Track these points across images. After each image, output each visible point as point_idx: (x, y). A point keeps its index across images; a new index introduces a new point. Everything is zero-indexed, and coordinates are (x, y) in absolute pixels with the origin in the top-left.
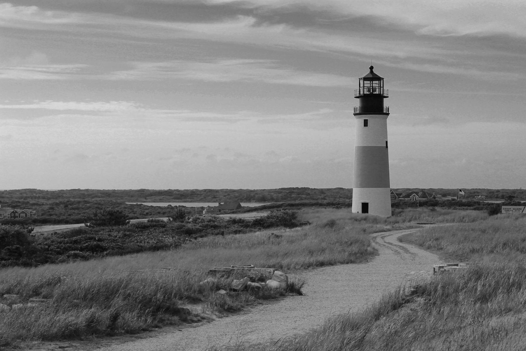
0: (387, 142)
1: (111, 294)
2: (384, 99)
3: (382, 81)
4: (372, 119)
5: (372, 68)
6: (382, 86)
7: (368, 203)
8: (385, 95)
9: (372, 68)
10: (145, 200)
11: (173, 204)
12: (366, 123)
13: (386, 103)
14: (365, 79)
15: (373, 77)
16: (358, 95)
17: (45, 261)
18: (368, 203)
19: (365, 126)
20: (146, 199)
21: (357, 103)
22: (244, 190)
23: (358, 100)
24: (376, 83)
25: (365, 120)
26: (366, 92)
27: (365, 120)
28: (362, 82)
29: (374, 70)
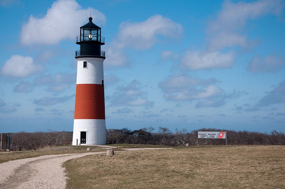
0: (103, 81)
3: (99, 31)
5: (91, 19)
6: (99, 34)
7: (86, 132)
8: (102, 42)
9: (91, 19)
13: (102, 48)
14: (84, 28)
15: (90, 26)
16: (79, 41)
19: (84, 67)
21: (78, 48)
23: (79, 46)
25: (84, 62)
27: (84, 62)
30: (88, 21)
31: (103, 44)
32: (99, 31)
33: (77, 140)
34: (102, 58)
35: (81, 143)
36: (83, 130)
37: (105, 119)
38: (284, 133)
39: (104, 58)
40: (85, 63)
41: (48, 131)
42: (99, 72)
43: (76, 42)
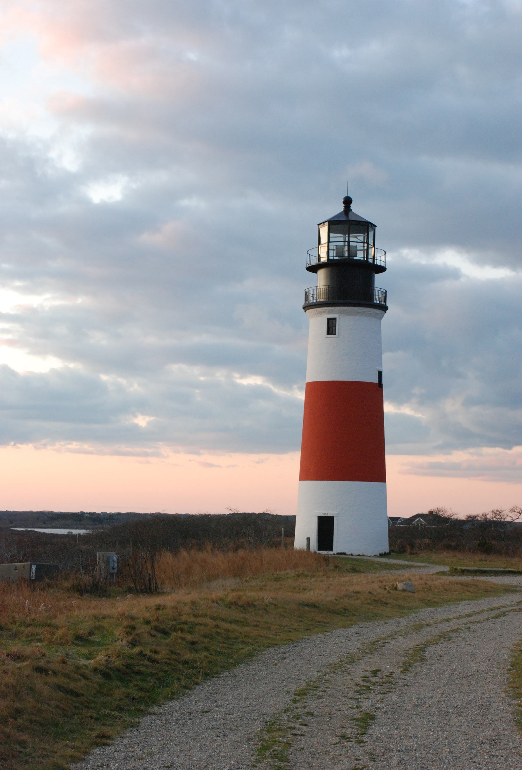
0: (380, 373)
1: (6, 629)
2: (378, 278)
3: (371, 234)
4: (348, 319)
5: (348, 201)
7: (332, 518)
9: (348, 201)
10: (44, 525)
11: (75, 532)
12: (331, 327)
14: (334, 225)
15: (346, 223)
16: (314, 262)
17: (446, 575)
18: (332, 518)
19: (329, 333)
20: (45, 523)
21: (320, 281)
22: (142, 514)
24: (357, 240)
25: (329, 320)
26: (333, 255)
27: (329, 320)
28: (324, 231)
29: (353, 207)
30: (341, 208)
31: (382, 269)
32: (370, 233)
33: (308, 539)
34: (379, 309)
35: (320, 549)
36: (325, 512)
37: (384, 481)
38: (85, 73)
39: (385, 308)
40: (330, 321)
41: (227, 512)
42: (400, 591)
43: (305, 266)
